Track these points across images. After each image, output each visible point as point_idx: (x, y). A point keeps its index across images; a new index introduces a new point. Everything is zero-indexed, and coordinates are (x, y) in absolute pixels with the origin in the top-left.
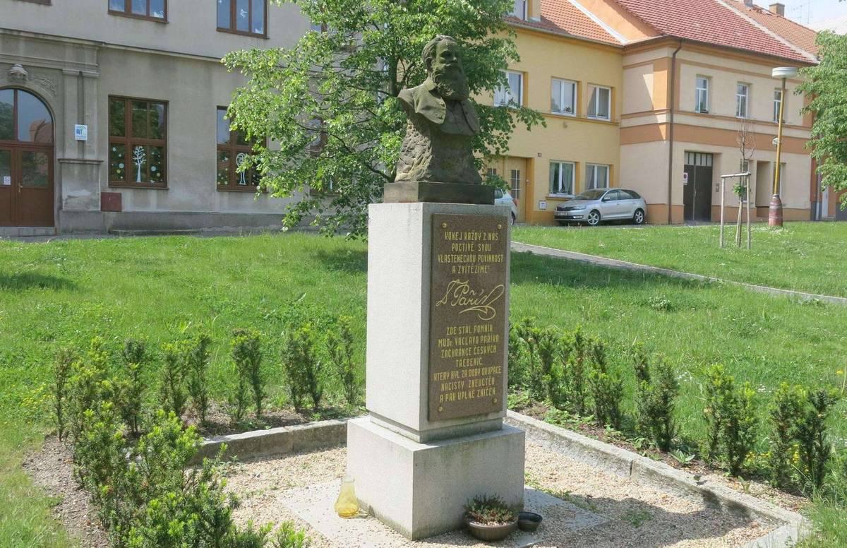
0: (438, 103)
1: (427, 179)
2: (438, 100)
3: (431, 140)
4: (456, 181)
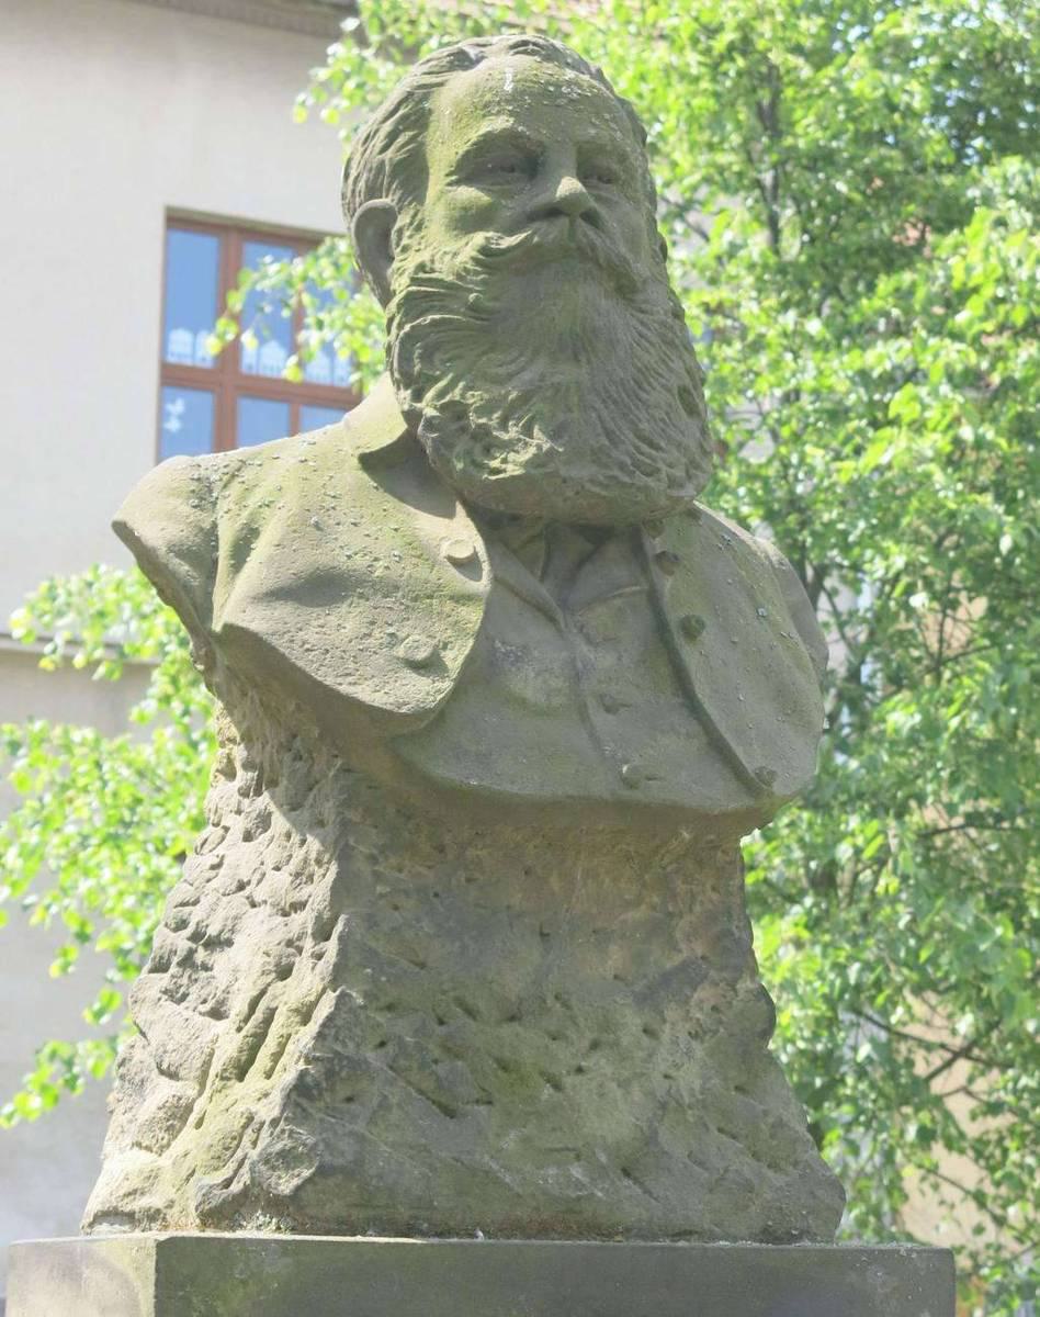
0: (422, 552)
1: (277, 1206)
2: (427, 525)
3: (343, 855)
4: (570, 1219)
